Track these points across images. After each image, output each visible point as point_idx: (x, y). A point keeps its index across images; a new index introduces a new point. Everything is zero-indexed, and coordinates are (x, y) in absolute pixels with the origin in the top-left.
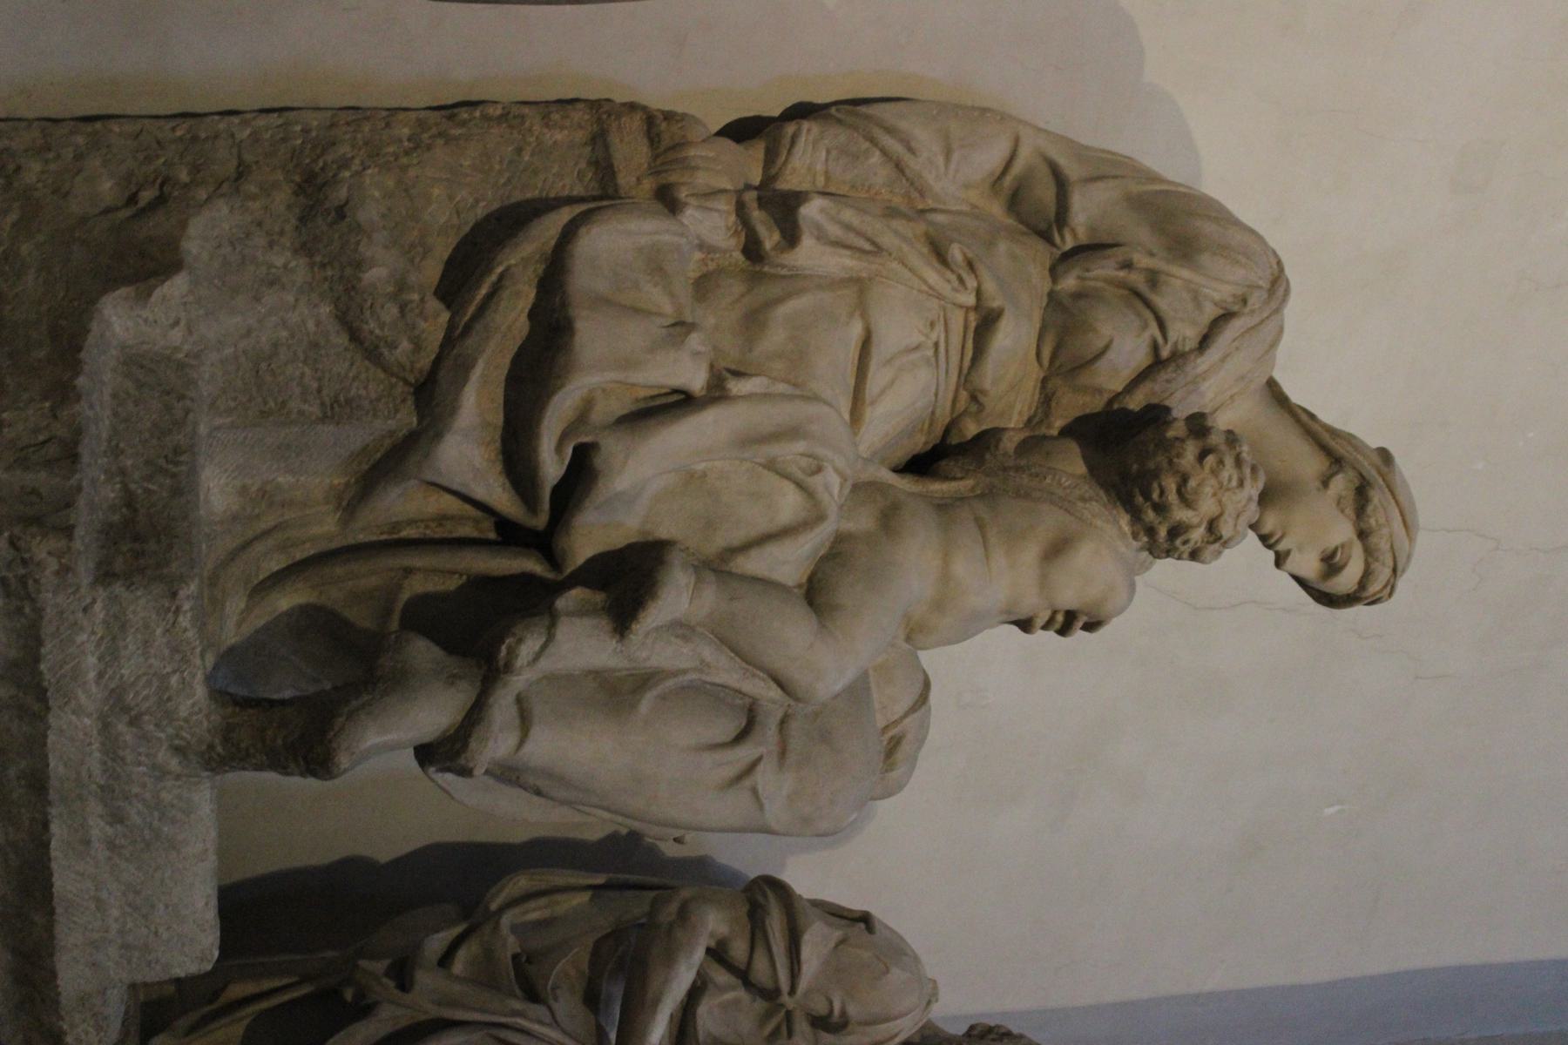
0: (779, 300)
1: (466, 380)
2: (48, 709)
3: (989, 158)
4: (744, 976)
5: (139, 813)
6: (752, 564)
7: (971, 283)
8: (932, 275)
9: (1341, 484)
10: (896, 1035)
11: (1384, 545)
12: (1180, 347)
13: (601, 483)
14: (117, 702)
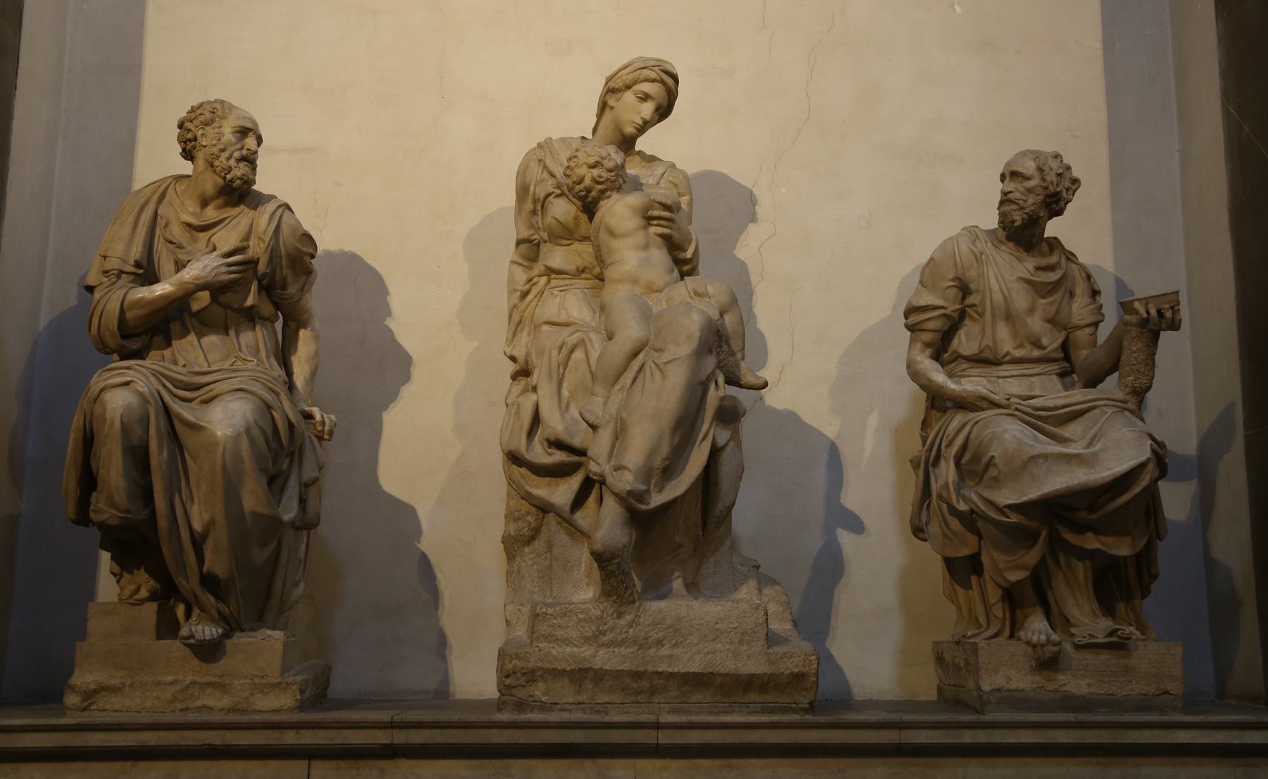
2: (590, 668)
5: (657, 633)
7: (535, 280)
10: (971, 250)
12: (555, 186)
14: (594, 639)
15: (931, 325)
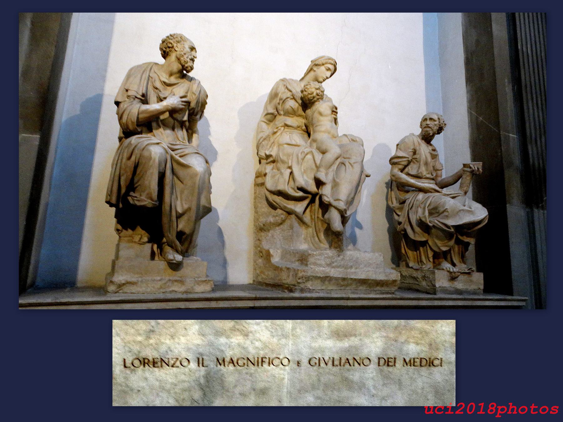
0: (280, 158)
1: (287, 207)
3: (264, 125)
4: (406, 166)
6: (318, 162)
7: (280, 128)
8: (278, 134)
9: (315, 68)
11: (325, 61)
13: (303, 186)
14: (329, 265)
15: (403, 163)
